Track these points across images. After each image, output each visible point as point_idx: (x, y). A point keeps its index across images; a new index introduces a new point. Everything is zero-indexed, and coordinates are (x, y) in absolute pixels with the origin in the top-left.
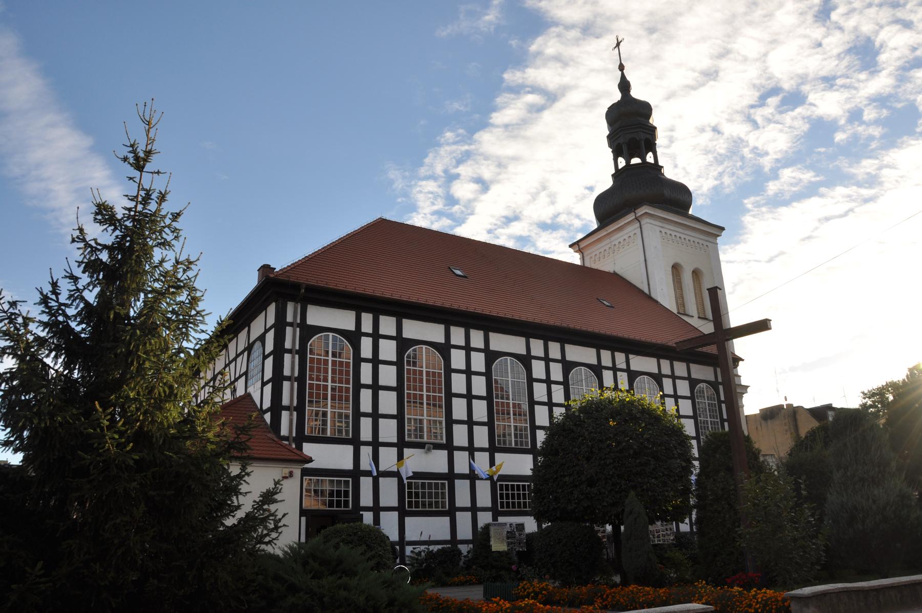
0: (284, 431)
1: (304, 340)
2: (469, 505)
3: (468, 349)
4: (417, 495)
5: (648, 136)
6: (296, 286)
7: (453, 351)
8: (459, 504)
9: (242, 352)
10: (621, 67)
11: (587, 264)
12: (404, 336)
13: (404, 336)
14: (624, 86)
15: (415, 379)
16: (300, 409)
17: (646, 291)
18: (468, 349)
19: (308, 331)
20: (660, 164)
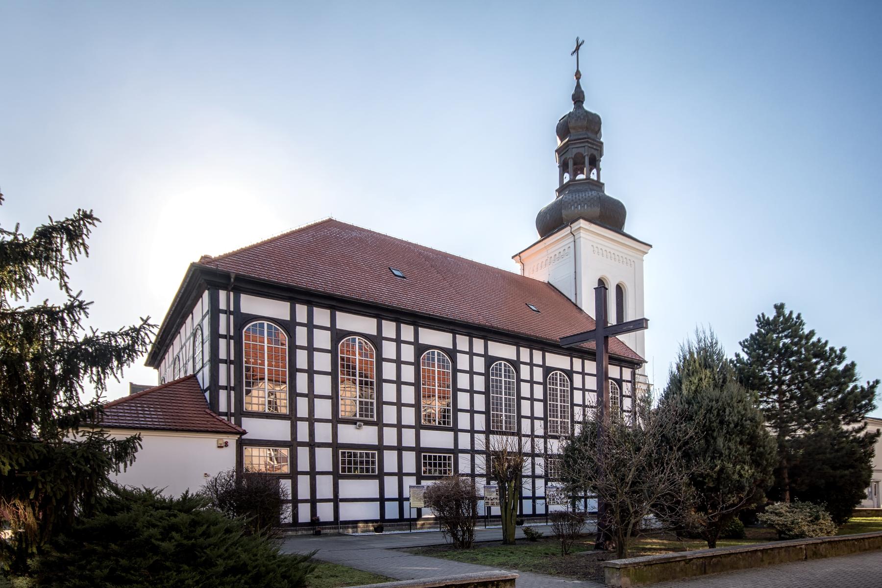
0: (223, 408)
1: (239, 328)
2: (396, 471)
3: (471, 354)
4: (350, 463)
5: (595, 153)
6: (227, 276)
7: (298, 328)
8: (386, 469)
9: (189, 338)
10: (578, 75)
11: (526, 275)
12: (420, 342)
13: (420, 342)
14: (578, 98)
15: (429, 377)
16: (238, 388)
17: (573, 300)
18: (398, 341)
19: (242, 320)
20: (602, 181)
